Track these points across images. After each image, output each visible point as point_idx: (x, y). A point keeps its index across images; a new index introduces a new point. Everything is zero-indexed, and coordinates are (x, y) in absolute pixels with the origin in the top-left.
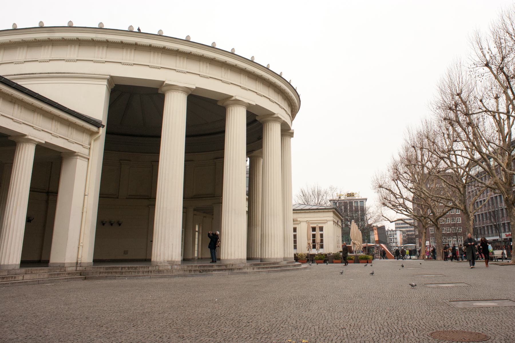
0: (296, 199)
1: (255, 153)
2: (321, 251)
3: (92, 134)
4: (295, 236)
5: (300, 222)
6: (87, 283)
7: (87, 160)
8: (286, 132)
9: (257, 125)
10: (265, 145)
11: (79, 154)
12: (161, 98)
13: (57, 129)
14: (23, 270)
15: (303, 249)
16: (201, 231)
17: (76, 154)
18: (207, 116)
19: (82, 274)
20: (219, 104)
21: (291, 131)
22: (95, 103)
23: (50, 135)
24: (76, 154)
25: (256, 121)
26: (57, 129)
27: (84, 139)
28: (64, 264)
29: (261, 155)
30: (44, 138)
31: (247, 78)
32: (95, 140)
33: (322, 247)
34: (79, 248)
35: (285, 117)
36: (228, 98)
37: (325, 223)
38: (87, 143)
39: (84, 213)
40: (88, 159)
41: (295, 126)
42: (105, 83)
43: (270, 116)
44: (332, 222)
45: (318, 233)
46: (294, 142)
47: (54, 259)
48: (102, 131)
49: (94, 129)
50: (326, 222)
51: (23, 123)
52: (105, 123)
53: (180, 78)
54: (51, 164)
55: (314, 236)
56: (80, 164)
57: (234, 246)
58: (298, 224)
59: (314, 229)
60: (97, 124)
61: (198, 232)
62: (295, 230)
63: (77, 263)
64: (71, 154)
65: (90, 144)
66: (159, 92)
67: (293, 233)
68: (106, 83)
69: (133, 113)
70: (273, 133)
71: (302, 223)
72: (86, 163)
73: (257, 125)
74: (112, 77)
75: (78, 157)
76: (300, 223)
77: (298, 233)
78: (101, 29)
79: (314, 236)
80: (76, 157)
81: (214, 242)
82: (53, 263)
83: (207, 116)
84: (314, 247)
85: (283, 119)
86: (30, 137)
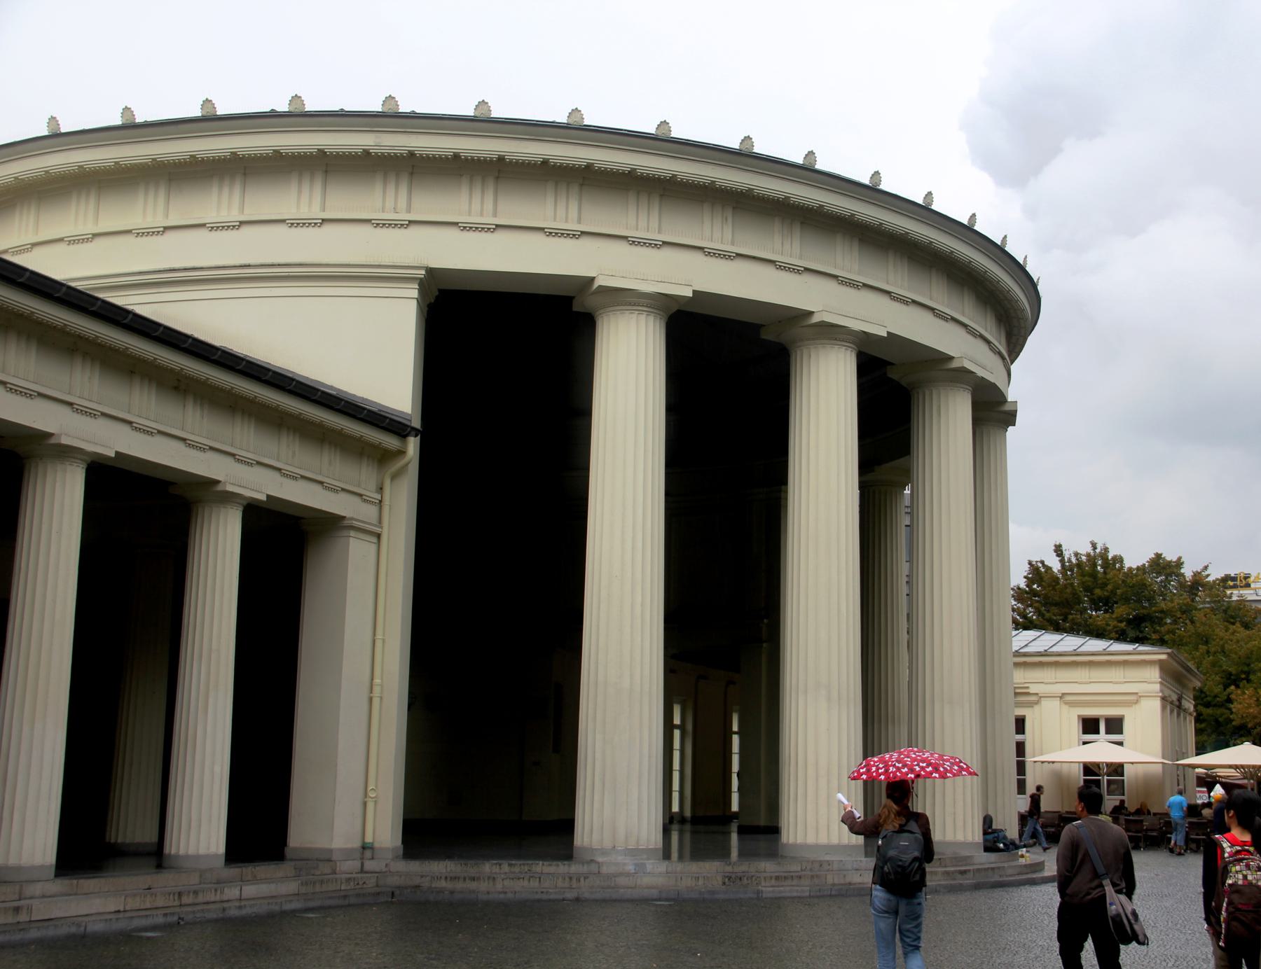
1: (883, 472)
3: (383, 457)
4: (1020, 748)
5: (1039, 698)
7: (375, 540)
8: (993, 412)
9: (891, 397)
11: (356, 523)
13: (294, 453)
14: (234, 871)
16: (689, 727)
17: (346, 523)
18: (729, 380)
20: (766, 335)
21: (1007, 408)
22: (378, 359)
23: (276, 475)
24: (346, 523)
26: (294, 453)
27: (364, 476)
28: (330, 851)
29: (906, 476)
31: (856, 244)
32: (394, 477)
34: (365, 804)
36: (798, 317)
37: (1128, 704)
38: (372, 485)
39: (376, 702)
40: (379, 536)
41: (1024, 383)
43: (934, 365)
44: (1157, 703)
47: (301, 834)
48: (413, 446)
49: (390, 442)
50: (1135, 699)
51: (212, 448)
52: (416, 423)
53: (639, 262)
54: (283, 549)
56: (357, 550)
57: (820, 793)
58: (1031, 705)
61: (682, 728)
62: (1020, 724)
63: (364, 847)
64: (329, 524)
65: (380, 489)
66: (576, 307)
67: (1014, 759)
68: (415, 293)
69: (502, 360)
70: (948, 426)
71: (1044, 702)
72: (373, 548)
74: (431, 272)
75: (352, 533)
76: (1037, 703)
77: (1029, 737)
80: (345, 533)
82: (295, 849)
83: (729, 380)
85: (980, 372)
86: (230, 488)
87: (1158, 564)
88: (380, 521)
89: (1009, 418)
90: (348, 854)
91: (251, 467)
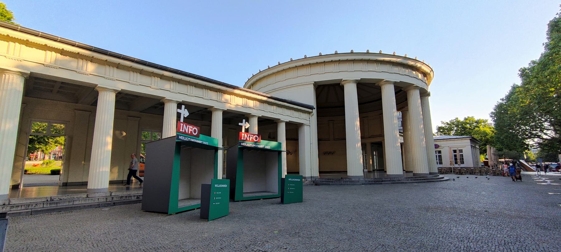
0: (436, 122)
2: (462, 166)
3: (309, 113)
6: (317, 187)
8: (424, 94)
9: (402, 93)
10: (409, 105)
12: (342, 88)
15: (447, 162)
18: (369, 93)
19: (315, 183)
20: (376, 84)
22: (309, 97)
25: (401, 90)
27: (305, 116)
30: (288, 119)
33: (463, 163)
35: (421, 85)
41: (430, 89)
42: (312, 86)
43: (410, 86)
45: (458, 154)
46: (431, 100)
48: (315, 111)
49: (310, 110)
52: (315, 107)
53: (349, 76)
54: (293, 130)
55: (455, 156)
59: (455, 151)
60: (311, 108)
64: (301, 125)
69: (329, 97)
70: (414, 98)
73: (402, 93)
78: (368, 53)
79: (455, 156)
81: (382, 168)
83: (369, 93)
84: (456, 163)
87: (466, 119)
88: (8, 50)
89: (429, 95)
90: (309, 177)
91: (285, 116)
